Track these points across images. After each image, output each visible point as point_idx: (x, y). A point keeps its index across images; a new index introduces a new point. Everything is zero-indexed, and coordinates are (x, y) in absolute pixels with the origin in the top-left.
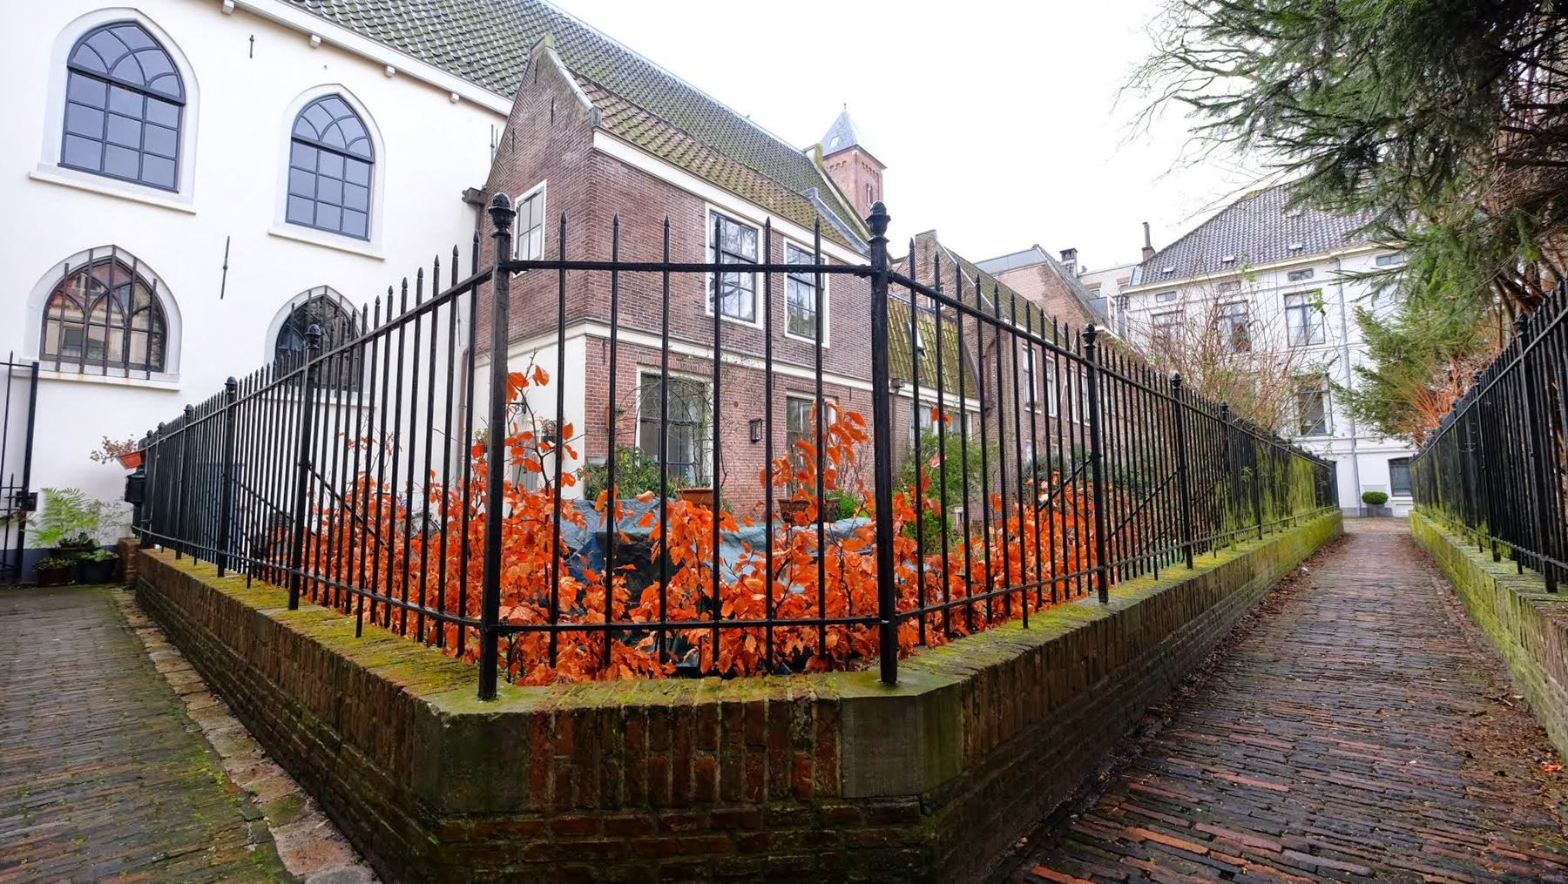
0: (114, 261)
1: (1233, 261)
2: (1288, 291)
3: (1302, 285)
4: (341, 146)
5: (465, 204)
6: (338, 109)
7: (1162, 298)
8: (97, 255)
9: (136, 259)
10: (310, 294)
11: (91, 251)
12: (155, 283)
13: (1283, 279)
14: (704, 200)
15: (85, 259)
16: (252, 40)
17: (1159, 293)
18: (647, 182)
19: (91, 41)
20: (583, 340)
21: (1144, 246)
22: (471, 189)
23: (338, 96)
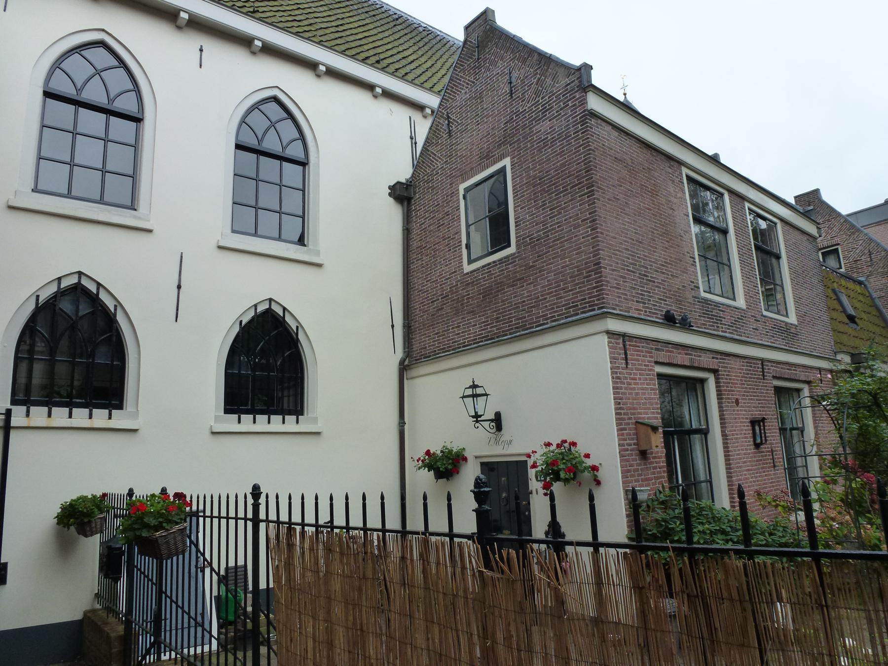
4: (277, 148)
5: (391, 200)
6: (100, 57)
8: (65, 284)
9: (99, 285)
10: (256, 309)
12: (115, 310)
14: (680, 163)
15: (53, 289)
16: (201, 50)
18: (636, 146)
19: (65, 65)
20: (605, 339)
22: (398, 183)
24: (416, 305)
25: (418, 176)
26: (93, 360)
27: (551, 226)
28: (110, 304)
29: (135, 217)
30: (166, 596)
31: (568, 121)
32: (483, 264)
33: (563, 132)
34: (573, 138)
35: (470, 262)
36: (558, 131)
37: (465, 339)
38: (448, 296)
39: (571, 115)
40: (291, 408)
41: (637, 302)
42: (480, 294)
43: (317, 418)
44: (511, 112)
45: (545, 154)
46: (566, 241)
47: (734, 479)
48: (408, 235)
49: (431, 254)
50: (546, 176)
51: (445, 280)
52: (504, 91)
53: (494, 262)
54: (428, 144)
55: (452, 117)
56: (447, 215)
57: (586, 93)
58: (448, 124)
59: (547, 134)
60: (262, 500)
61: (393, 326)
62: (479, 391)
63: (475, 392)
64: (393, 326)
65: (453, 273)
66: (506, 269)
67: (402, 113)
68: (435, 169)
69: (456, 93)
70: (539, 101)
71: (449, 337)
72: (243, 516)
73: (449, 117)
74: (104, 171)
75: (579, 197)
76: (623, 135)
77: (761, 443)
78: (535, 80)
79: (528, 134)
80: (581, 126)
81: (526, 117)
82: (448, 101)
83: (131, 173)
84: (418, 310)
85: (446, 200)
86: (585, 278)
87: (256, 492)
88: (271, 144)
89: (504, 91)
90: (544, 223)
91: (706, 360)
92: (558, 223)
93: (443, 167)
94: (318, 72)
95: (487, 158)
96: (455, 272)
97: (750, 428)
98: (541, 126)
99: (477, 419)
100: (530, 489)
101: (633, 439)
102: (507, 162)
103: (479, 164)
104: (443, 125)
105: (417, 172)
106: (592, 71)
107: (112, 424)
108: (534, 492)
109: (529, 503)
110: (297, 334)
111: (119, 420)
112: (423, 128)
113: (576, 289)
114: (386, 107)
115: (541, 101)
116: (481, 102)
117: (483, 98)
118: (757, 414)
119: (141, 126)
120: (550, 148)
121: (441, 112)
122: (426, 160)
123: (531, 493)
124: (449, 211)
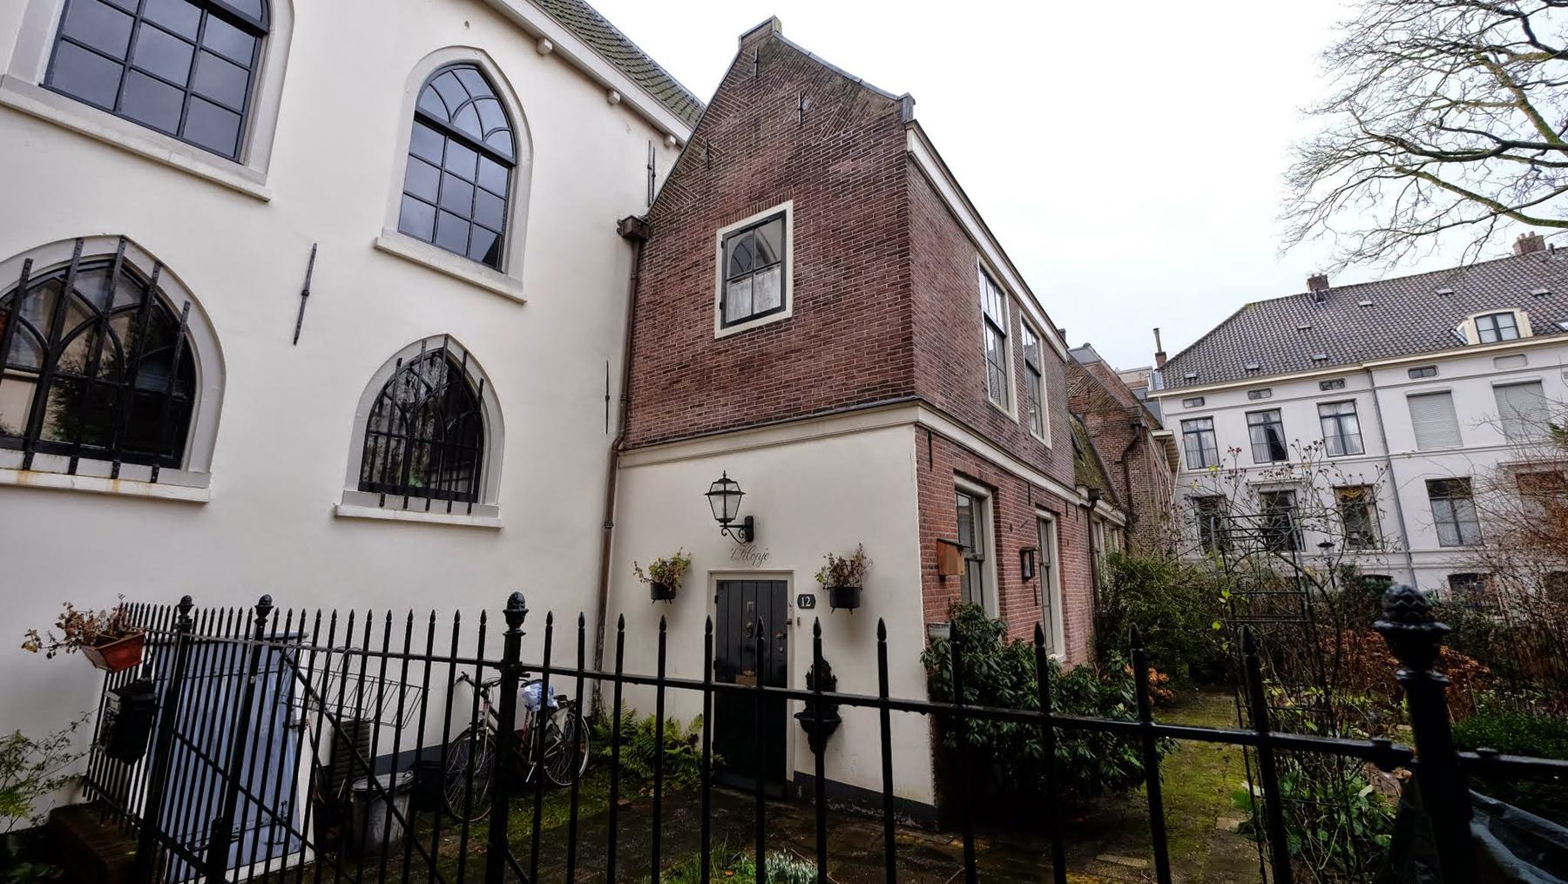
0: (118, 268)
1: (1195, 378)
3: (1334, 394)
4: (474, 133)
5: (620, 238)
6: (478, 87)
7: (1188, 404)
8: (88, 251)
11: (79, 241)
12: (186, 309)
13: (1314, 389)
17: (1187, 398)
21: (1157, 351)
22: (632, 217)
23: (478, 67)
24: (638, 374)
25: (657, 214)
26: (132, 383)
27: (844, 289)
28: (177, 300)
29: (240, 175)
30: (249, 797)
31: (879, 163)
32: (744, 329)
33: (871, 176)
34: (884, 184)
35: (725, 325)
36: (863, 174)
37: (709, 422)
38: (689, 366)
39: (884, 156)
40: (459, 491)
41: (941, 394)
43: (498, 508)
44: (799, 146)
45: (843, 201)
46: (866, 308)
47: (1008, 616)
48: (636, 286)
49: (669, 312)
50: (842, 228)
51: (687, 345)
52: (790, 119)
53: (759, 328)
54: (675, 176)
55: (712, 145)
56: (696, 266)
57: (906, 130)
58: (708, 153)
59: (848, 176)
60: (270, 617)
61: (608, 398)
62: (729, 487)
63: (725, 489)
64: (608, 398)
65: (698, 338)
66: (777, 337)
67: (638, 141)
69: (721, 117)
70: (840, 135)
71: (686, 418)
72: (424, 653)
73: (709, 145)
74: (187, 92)
75: (888, 255)
76: (934, 196)
77: (1029, 578)
78: (836, 110)
79: (820, 175)
80: (897, 170)
81: (819, 153)
82: (709, 125)
83: (239, 108)
84: (642, 382)
85: (696, 247)
86: (888, 355)
87: (264, 606)
88: (466, 124)
89: (790, 119)
90: (835, 284)
91: (991, 477)
92: (856, 285)
93: (695, 205)
94: (541, 49)
95: (759, 199)
96: (702, 336)
97: (1019, 559)
98: (840, 166)
99: (725, 524)
100: (789, 617)
101: (934, 561)
102: (788, 206)
103: (748, 206)
104: (700, 155)
105: (656, 209)
106: (914, 106)
107: (157, 490)
108: (795, 623)
109: (785, 636)
110: (480, 391)
111: (170, 485)
112: (666, 163)
113: (875, 368)
114: (614, 123)
115: (842, 135)
116: (756, 131)
117: (759, 125)
119: (264, 42)
120: (851, 193)
121: (697, 138)
122: (670, 195)
124: (698, 261)
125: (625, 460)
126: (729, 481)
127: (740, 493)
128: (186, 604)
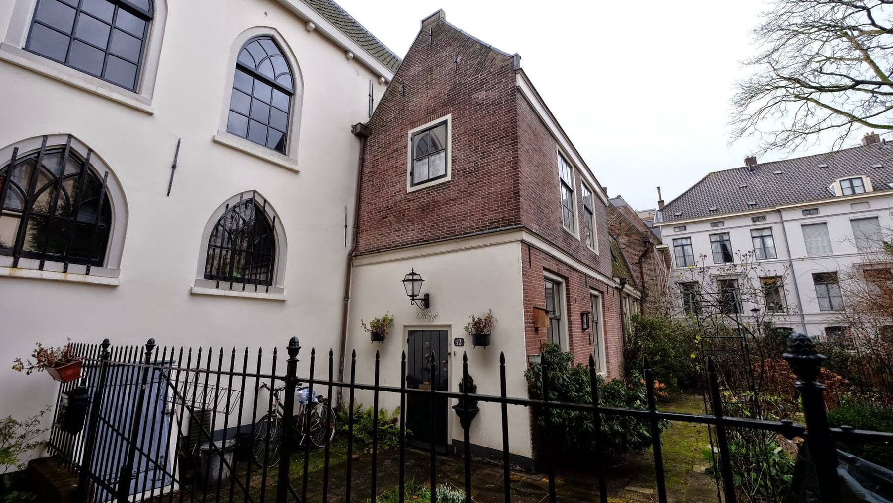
1: (681, 215)
2: (675, 237)
3: (760, 224)
4: (270, 76)
5: (353, 135)
6: (272, 49)
7: (677, 230)
8: (50, 143)
11: (45, 137)
12: (106, 176)
13: (748, 221)
17: (676, 227)
21: (659, 200)
22: (360, 123)
23: (272, 38)
25: (374, 122)
26: (75, 218)
27: (481, 164)
28: (101, 171)
29: (137, 99)
30: (142, 453)
31: (501, 93)
32: (424, 187)
33: (496, 100)
34: (503, 105)
35: (413, 185)
37: (404, 240)
38: (392, 208)
39: (503, 89)
41: (536, 224)
42: (419, 208)
43: (283, 289)
44: (455, 83)
45: (480, 114)
46: (493, 175)
48: (362, 163)
49: (381, 177)
51: (391, 197)
52: (450, 68)
53: (433, 186)
54: (384, 100)
55: (406, 82)
56: (396, 151)
57: (516, 74)
58: (403, 87)
59: (483, 100)
60: (154, 351)
61: (346, 226)
62: (415, 277)
63: (413, 278)
64: (346, 226)
65: (398, 192)
66: (443, 192)
67: (363, 80)
68: (388, 118)
69: (410, 66)
70: (478, 77)
71: (391, 238)
72: (241, 371)
74: (107, 52)
75: (506, 145)
76: (532, 111)
77: (586, 329)
78: (476, 62)
79: (467, 99)
80: (511, 97)
81: (467, 87)
82: (404, 71)
83: (136, 61)
84: (366, 217)
85: (396, 140)
86: (506, 202)
87: (150, 345)
89: (450, 68)
91: (565, 271)
92: (488, 162)
93: (396, 117)
94: (308, 28)
95: (432, 113)
96: (400, 191)
97: (580, 318)
99: (413, 298)
100: (449, 351)
102: (449, 117)
103: (426, 117)
104: (398, 88)
105: (374, 119)
106: (521, 61)
107: (89, 279)
108: (453, 354)
109: (447, 362)
110: (274, 222)
111: (97, 276)
112: (380, 93)
113: (498, 209)
114: (350, 70)
115: (480, 77)
116: (430, 75)
117: (432, 71)
118: (584, 309)
119: (150, 24)
120: (484, 110)
121: (397, 79)
122: (382, 111)
123: (450, 354)
124: (398, 148)
125: (356, 262)
126: (415, 274)
127: (421, 281)
128: (106, 344)
